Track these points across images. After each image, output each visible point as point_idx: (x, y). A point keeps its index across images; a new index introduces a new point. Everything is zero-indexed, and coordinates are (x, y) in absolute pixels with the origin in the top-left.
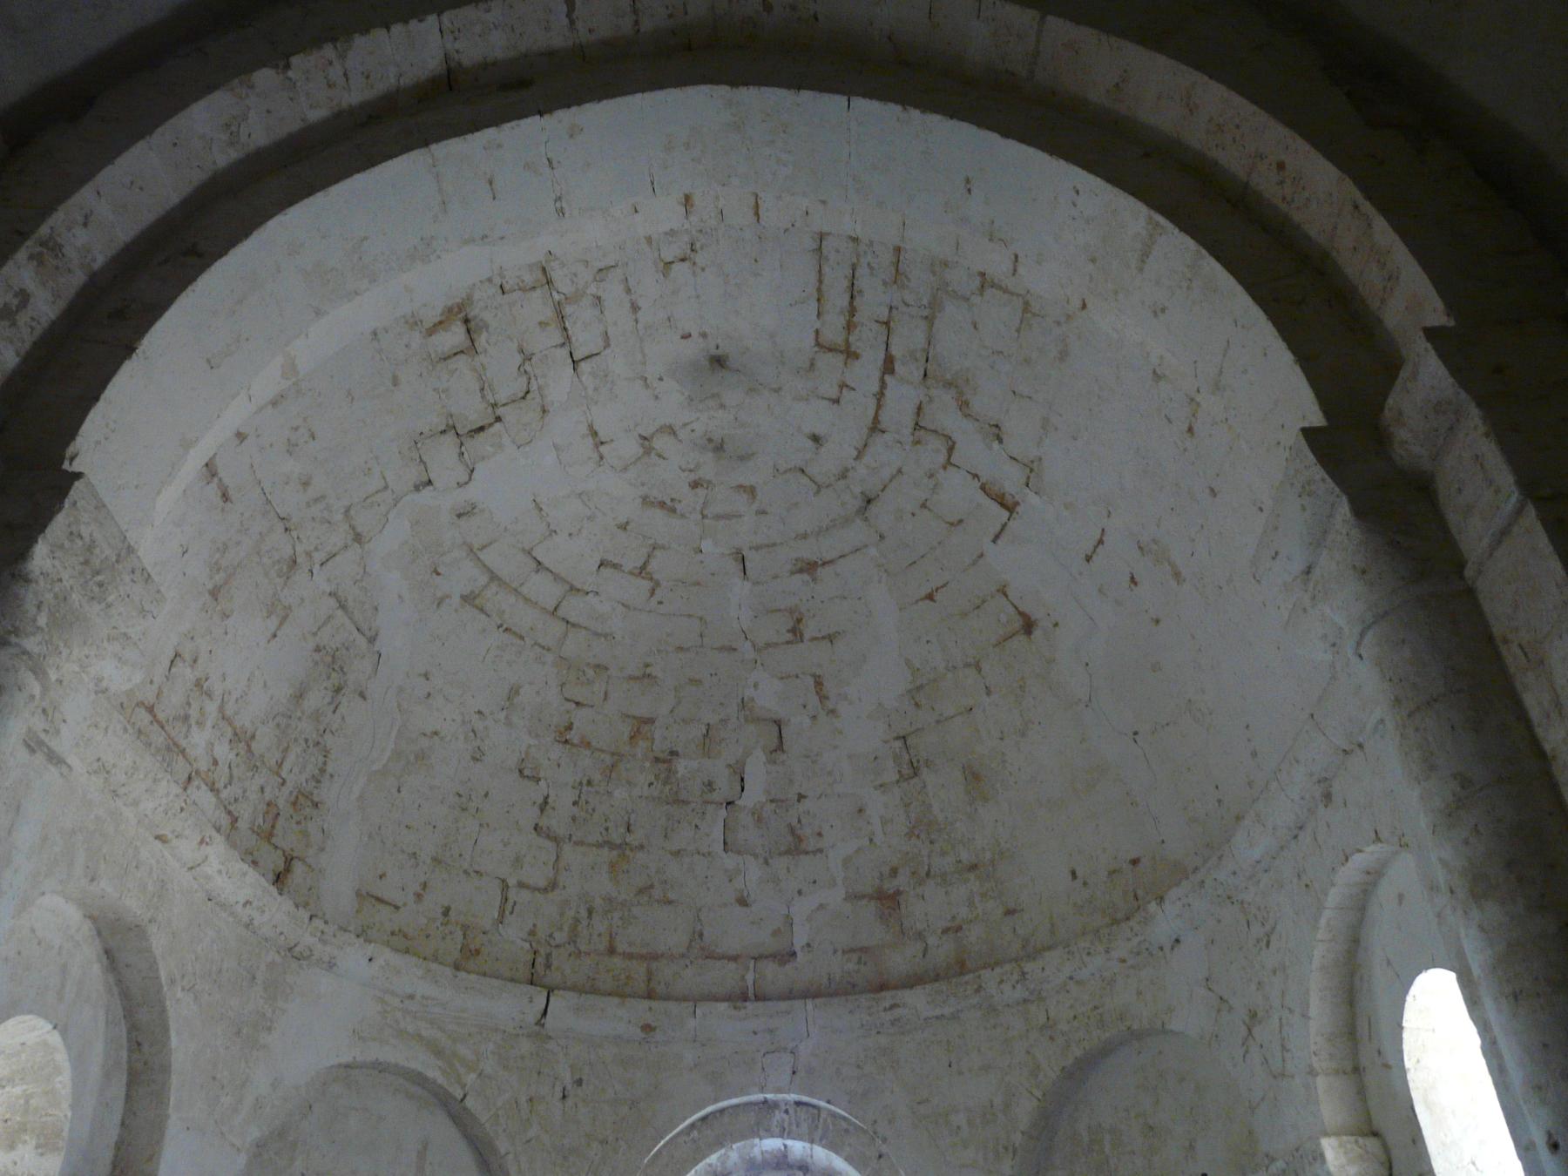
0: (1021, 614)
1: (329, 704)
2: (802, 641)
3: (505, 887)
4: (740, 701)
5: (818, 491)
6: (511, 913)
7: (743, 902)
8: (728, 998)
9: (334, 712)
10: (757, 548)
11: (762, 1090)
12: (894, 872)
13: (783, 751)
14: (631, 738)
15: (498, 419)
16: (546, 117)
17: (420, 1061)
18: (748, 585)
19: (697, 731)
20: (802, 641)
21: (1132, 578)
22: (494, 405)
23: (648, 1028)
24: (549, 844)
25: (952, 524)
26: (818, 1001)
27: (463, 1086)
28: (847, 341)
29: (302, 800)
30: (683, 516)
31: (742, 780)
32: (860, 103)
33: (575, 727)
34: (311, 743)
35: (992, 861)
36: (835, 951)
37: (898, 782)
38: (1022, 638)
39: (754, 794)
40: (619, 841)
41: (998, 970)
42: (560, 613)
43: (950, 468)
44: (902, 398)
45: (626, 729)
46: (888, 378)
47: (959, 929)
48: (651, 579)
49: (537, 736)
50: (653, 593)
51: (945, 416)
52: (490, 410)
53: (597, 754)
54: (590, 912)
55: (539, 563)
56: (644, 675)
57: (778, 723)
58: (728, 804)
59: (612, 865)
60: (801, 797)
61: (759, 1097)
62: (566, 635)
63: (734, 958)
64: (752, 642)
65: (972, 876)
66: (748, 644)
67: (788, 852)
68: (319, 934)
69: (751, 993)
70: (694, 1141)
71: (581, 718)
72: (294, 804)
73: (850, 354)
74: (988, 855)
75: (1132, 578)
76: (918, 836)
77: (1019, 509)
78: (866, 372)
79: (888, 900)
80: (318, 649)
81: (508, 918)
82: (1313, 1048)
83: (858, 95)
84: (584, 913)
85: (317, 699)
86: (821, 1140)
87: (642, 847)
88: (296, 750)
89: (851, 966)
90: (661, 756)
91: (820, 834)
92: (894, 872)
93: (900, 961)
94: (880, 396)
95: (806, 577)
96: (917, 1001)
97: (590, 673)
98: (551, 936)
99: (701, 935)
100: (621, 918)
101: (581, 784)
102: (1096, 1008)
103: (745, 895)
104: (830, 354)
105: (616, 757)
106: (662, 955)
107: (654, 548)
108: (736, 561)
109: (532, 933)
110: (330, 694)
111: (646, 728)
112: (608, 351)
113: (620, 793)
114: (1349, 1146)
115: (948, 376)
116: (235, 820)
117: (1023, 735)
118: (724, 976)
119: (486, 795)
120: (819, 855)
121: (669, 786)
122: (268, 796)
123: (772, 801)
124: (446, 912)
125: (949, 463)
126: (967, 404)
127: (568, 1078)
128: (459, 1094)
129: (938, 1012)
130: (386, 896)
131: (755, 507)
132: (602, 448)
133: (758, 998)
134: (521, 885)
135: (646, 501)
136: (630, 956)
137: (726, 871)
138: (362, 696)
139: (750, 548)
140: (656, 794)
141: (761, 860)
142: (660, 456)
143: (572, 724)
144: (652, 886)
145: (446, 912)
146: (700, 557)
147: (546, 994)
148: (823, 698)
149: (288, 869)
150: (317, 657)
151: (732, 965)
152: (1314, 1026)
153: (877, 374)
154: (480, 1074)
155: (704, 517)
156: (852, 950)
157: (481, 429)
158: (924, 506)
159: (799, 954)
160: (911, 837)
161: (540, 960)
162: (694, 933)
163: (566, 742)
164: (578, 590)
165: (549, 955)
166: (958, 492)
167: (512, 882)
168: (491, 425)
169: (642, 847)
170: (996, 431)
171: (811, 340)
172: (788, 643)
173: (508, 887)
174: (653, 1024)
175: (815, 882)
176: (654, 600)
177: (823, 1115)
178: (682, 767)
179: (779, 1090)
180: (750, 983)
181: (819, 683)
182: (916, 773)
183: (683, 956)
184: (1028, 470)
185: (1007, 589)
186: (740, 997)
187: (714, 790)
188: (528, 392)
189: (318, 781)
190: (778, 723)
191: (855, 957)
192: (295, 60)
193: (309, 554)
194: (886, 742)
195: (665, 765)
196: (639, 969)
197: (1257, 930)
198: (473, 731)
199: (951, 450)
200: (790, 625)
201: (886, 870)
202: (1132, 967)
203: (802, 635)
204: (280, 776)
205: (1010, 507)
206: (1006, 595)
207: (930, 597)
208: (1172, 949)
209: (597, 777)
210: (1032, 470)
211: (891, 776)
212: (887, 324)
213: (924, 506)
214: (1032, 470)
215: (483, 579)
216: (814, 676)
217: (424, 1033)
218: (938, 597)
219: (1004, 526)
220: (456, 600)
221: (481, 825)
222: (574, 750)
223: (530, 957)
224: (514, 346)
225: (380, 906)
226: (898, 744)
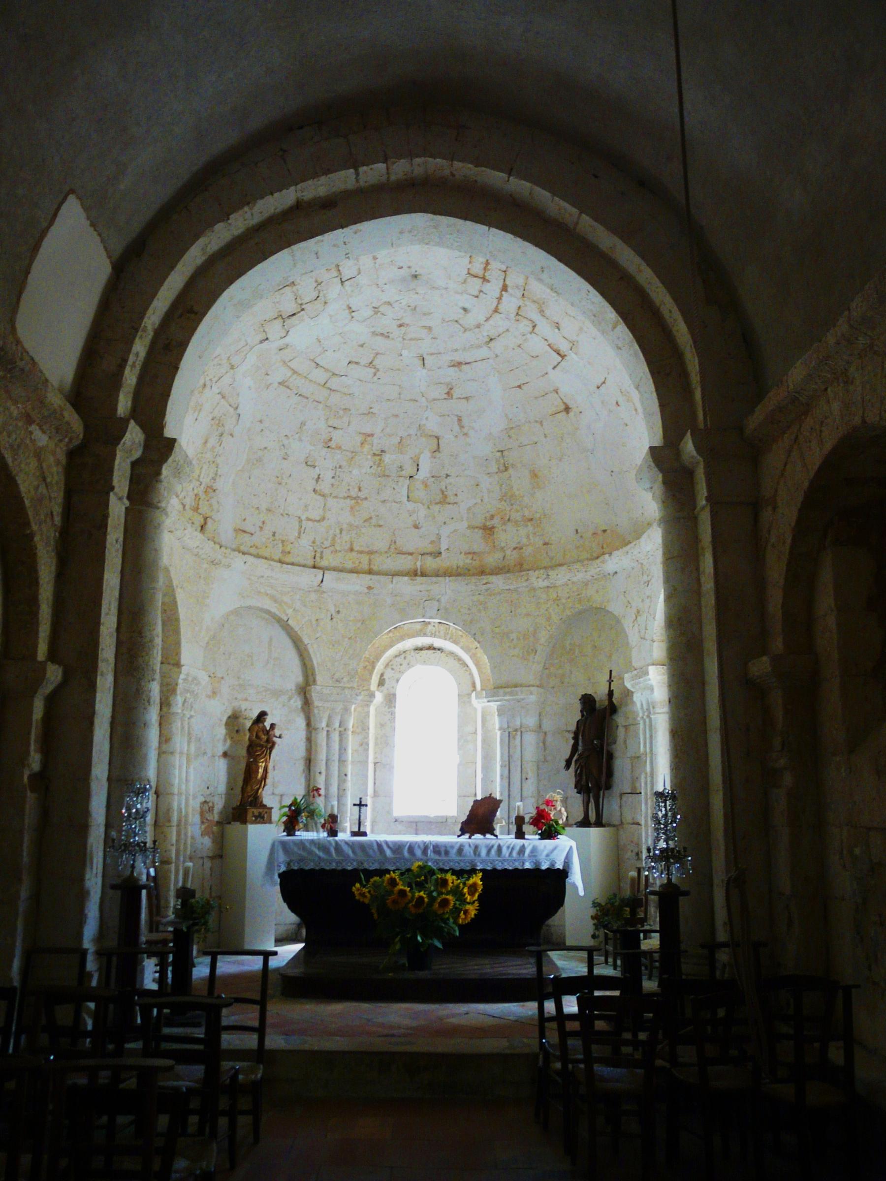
0: (565, 403)
1: (218, 442)
2: (452, 399)
3: (300, 521)
4: (418, 426)
5: (465, 331)
6: (304, 533)
7: (416, 527)
8: (407, 574)
9: (220, 446)
10: (432, 354)
11: (423, 617)
12: (492, 517)
13: (439, 452)
14: (362, 444)
15: (303, 310)
16: (345, 229)
17: (268, 605)
18: (425, 371)
19: (396, 440)
20: (452, 399)
21: (617, 403)
22: (301, 304)
23: (369, 588)
24: (321, 498)
25: (533, 357)
26: (451, 578)
27: (287, 615)
28: (484, 274)
29: (209, 490)
30: (393, 339)
31: (418, 465)
32: (494, 230)
33: (333, 439)
34: (211, 463)
35: (540, 518)
36: (461, 553)
37: (497, 473)
38: (564, 413)
39: (423, 474)
40: (355, 496)
41: (537, 572)
42: (327, 385)
43: (533, 334)
44: (510, 303)
45: (359, 439)
46: (503, 293)
47: (521, 548)
48: (375, 368)
49: (314, 445)
50: (375, 374)
51: (531, 312)
52: (299, 306)
53: (344, 452)
54: (341, 530)
55: (318, 364)
56: (369, 413)
57: (438, 438)
58: (411, 477)
59: (352, 508)
60: (447, 476)
61: (423, 620)
62: (329, 395)
63: (411, 554)
64: (426, 398)
65: (529, 524)
66: (424, 399)
67: (440, 503)
68: (223, 554)
69: (419, 573)
70: (390, 637)
71: (337, 435)
72: (206, 492)
73: (485, 279)
74: (538, 515)
75: (617, 403)
76: (505, 501)
77: (566, 358)
78: (493, 289)
79: (488, 530)
80: (213, 419)
81: (303, 536)
82: (655, 631)
83: (493, 227)
84: (338, 531)
85: (212, 441)
86: (450, 639)
87: (366, 499)
88: (205, 467)
89: (468, 561)
90: (377, 453)
91: (456, 495)
92: (492, 517)
93: (492, 559)
94: (500, 299)
95: (456, 369)
96: (498, 582)
97: (341, 412)
98: (322, 543)
99: (395, 542)
100: (356, 534)
101: (336, 468)
102: (578, 595)
103: (418, 523)
104: (475, 278)
105: (354, 454)
106: (376, 552)
107: (377, 354)
108: (419, 360)
109: (314, 542)
110: (218, 437)
111: (369, 438)
112: (360, 276)
113: (355, 472)
114: (660, 669)
115: (535, 299)
116: (184, 506)
117: (560, 460)
118: (406, 563)
119: (290, 476)
120: (455, 505)
121: (380, 468)
122: (196, 492)
123: (433, 477)
124: (274, 534)
125: (532, 332)
126: (543, 311)
127: (332, 610)
128: (285, 619)
129: (508, 587)
130: (247, 529)
131: (431, 336)
132: (353, 314)
133: (423, 575)
134: (308, 519)
135: (374, 334)
136: (361, 552)
137: (408, 511)
138: (232, 435)
139: (428, 354)
140: (374, 472)
141: (426, 507)
142: (382, 314)
143: (331, 438)
144: (371, 518)
145: (274, 534)
146: (401, 358)
147: (322, 573)
148: (462, 427)
149: (205, 523)
150: (213, 422)
151: (410, 557)
152: (656, 623)
153: (499, 291)
154: (294, 609)
155: (404, 339)
156: (470, 553)
157: (294, 314)
158: (519, 346)
159: (443, 554)
160: (501, 501)
161: (318, 555)
162: (392, 541)
163: (329, 447)
164: (336, 375)
165: (322, 552)
166: (536, 344)
167: (303, 518)
168: (299, 312)
169: (366, 499)
170: (557, 325)
171: (466, 272)
172: (445, 399)
173: (302, 520)
174: (372, 586)
175: (452, 518)
176: (375, 378)
177: (451, 629)
178: (387, 458)
179: (431, 618)
180: (419, 567)
181: (460, 420)
182: (506, 469)
183: (386, 552)
184: (572, 344)
185: (558, 391)
186: (414, 574)
187: (403, 470)
188: (318, 297)
189: (215, 480)
190: (438, 438)
191: (470, 556)
192: (231, 216)
193: (211, 380)
194: (492, 452)
195: (379, 457)
196: (365, 559)
197: (645, 578)
198: (283, 445)
199: (534, 327)
200: (446, 391)
201: (488, 515)
202: (596, 579)
203: (452, 396)
204: (199, 481)
205: (563, 357)
206: (557, 393)
207: (519, 387)
208: (613, 575)
209: (344, 464)
210: (573, 345)
211: (494, 469)
212: (505, 271)
213: (519, 346)
214: (573, 345)
215: (289, 373)
216: (457, 416)
217: (269, 592)
218: (523, 387)
219: (559, 363)
220: (276, 384)
221: (288, 491)
222: (333, 451)
223: (313, 554)
224: (314, 280)
225: (245, 535)
226: (499, 454)
